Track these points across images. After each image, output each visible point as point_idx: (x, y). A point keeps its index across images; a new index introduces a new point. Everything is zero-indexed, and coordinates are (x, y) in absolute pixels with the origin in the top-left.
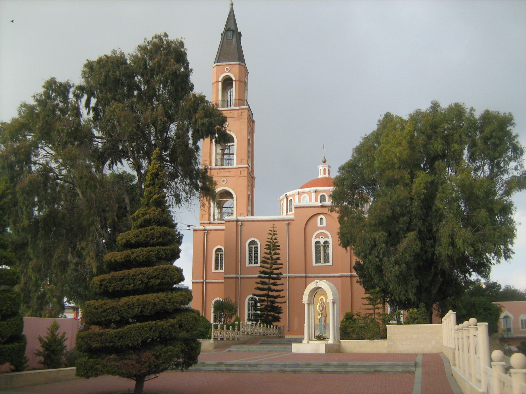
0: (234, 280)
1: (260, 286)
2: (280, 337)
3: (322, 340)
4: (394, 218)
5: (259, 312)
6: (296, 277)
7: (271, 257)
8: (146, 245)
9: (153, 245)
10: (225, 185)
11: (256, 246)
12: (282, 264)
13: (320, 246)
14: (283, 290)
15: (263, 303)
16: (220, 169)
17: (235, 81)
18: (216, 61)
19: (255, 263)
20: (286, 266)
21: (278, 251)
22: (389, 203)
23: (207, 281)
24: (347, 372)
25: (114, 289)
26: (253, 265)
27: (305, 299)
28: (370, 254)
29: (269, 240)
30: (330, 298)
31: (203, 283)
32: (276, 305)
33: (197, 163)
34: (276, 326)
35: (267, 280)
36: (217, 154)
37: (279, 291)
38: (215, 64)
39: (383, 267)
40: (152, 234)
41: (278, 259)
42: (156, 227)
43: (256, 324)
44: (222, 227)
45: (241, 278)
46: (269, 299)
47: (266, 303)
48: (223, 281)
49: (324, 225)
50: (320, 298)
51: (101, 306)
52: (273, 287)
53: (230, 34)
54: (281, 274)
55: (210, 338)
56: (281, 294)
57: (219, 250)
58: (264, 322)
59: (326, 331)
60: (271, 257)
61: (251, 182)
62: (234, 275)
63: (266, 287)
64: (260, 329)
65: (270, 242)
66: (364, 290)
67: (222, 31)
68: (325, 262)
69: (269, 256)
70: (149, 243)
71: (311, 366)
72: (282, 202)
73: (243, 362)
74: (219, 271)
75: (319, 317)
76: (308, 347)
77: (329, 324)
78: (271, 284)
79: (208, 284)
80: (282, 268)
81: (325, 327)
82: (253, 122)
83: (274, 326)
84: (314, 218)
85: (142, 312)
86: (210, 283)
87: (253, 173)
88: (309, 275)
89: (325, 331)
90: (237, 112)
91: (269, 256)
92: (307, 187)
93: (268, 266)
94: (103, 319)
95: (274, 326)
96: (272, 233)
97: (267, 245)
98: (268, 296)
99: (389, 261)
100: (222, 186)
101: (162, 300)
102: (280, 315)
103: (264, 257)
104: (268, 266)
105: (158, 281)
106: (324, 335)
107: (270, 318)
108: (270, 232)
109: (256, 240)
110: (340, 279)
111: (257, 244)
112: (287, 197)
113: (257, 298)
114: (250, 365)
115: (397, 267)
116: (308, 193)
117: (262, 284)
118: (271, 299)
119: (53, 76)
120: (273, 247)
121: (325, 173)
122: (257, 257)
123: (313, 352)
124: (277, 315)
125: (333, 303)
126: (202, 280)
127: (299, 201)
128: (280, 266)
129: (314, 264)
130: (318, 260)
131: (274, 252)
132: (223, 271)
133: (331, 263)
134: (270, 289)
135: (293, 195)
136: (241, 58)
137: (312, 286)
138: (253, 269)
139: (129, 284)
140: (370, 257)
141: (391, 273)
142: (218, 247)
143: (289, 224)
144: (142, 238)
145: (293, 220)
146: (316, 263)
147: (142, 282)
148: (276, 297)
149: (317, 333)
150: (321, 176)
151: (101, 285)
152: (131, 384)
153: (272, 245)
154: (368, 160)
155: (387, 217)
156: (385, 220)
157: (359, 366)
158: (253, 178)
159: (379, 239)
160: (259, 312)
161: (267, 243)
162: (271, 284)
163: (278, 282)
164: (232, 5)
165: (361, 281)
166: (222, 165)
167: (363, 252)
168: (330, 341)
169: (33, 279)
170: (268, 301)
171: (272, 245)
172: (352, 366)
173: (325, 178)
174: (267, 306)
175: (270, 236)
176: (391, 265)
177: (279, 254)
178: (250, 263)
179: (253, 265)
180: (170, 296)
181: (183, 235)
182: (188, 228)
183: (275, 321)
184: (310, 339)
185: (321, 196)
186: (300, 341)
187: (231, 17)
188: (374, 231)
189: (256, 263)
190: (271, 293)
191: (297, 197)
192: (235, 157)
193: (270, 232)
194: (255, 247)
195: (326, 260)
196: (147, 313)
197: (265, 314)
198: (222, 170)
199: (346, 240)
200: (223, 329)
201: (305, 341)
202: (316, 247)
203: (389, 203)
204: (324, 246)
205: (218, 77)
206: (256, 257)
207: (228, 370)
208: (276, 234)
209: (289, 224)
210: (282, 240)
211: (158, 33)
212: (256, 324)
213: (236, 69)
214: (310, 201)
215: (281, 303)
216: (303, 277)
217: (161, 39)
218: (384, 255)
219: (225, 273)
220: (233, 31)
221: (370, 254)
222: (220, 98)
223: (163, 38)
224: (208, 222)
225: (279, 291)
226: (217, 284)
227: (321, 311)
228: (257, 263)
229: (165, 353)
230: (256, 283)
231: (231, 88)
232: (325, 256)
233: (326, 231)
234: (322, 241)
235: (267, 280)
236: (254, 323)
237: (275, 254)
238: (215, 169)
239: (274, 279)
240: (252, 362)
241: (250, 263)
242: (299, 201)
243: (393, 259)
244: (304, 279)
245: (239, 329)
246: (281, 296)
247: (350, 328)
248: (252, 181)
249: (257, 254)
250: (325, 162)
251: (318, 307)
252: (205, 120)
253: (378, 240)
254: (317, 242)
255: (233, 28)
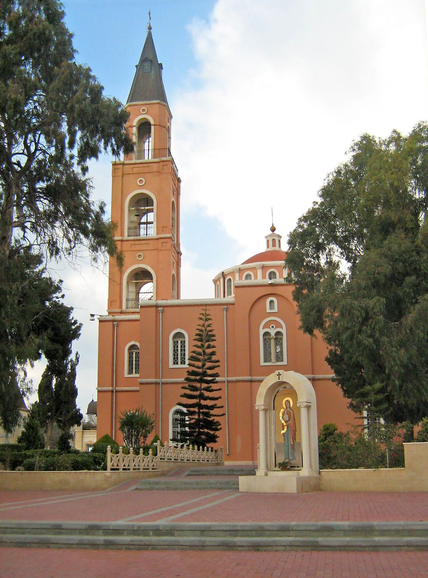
0: (154, 385)
1: (188, 392)
2: (218, 464)
3: (289, 470)
4: (396, 279)
5: (187, 429)
6: (238, 381)
7: (204, 351)
11: (182, 340)
12: (218, 361)
13: (270, 339)
14: (220, 398)
15: (193, 417)
16: (134, 240)
17: (154, 125)
18: (129, 100)
19: (181, 364)
20: (224, 364)
21: (212, 343)
23: (118, 388)
24: (375, 548)
26: (179, 366)
27: (260, 402)
28: (360, 331)
29: (200, 328)
34: (212, 448)
35: (198, 385)
37: (217, 399)
38: (128, 104)
39: (381, 352)
41: (213, 353)
43: (182, 447)
44: (137, 317)
45: (162, 384)
46: (201, 411)
47: (196, 417)
49: (276, 310)
52: (206, 394)
53: (147, 65)
54: (217, 375)
55: (105, 468)
56: (218, 403)
58: (193, 443)
60: (204, 351)
61: (176, 258)
62: (154, 380)
63: (197, 393)
64: (190, 453)
65: (201, 331)
66: (343, 393)
68: (277, 361)
69: (200, 350)
71: (291, 533)
72: (218, 283)
75: (283, 432)
76: (267, 480)
77: (300, 444)
78: (204, 389)
80: (219, 366)
81: (293, 447)
82: (179, 180)
83: (208, 448)
84: (262, 300)
86: (122, 391)
89: (293, 456)
90: (156, 165)
91: (200, 350)
93: (200, 364)
95: (208, 448)
97: (197, 335)
98: (200, 406)
99: (390, 343)
100: (137, 263)
102: (217, 433)
103: (194, 352)
104: (200, 364)
106: (293, 462)
107: (203, 437)
108: (201, 316)
111: (184, 337)
113: (185, 410)
114: (157, 531)
115: (403, 351)
116: (254, 269)
117: (191, 390)
118: (205, 410)
121: (274, 245)
124: (212, 432)
128: (216, 364)
131: (207, 344)
134: (202, 397)
137: (271, 380)
138: (179, 370)
141: (394, 360)
145: (233, 304)
146: (265, 361)
148: (212, 407)
149: (281, 459)
153: (204, 335)
156: (383, 280)
157: (398, 532)
160: (187, 429)
161: (198, 332)
162: (204, 389)
163: (214, 386)
164: (150, 28)
165: (338, 379)
168: (305, 472)
170: (199, 413)
172: (383, 532)
174: (198, 420)
176: (394, 349)
177: (214, 347)
178: (174, 364)
179: (179, 366)
181: (81, 324)
182: (92, 318)
183: (209, 442)
185: (271, 273)
186: (251, 472)
187: (149, 43)
189: (183, 362)
190: (203, 402)
193: (201, 316)
194: (181, 342)
197: (195, 432)
198: (138, 242)
200: (117, 452)
201: (261, 471)
202: (265, 340)
204: (276, 339)
207: (108, 544)
208: (210, 319)
210: (219, 328)
212: (182, 447)
215: (218, 416)
218: (382, 334)
224: (120, 310)
225: (217, 399)
227: (286, 422)
230: (183, 388)
231: (150, 137)
234: (273, 332)
235: (198, 385)
236: (180, 444)
237: (209, 347)
238: (128, 240)
239: (207, 382)
240: (162, 522)
241: (175, 363)
243: (396, 338)
244: (249, 384)
245: (155, 454)
246: (218, 405)
247: (333, 451)
248: (178, 257)
249: (184, 350)
251: (281, 415)
253: (373, 308)
254: (266, 334)
255: (151, 57)
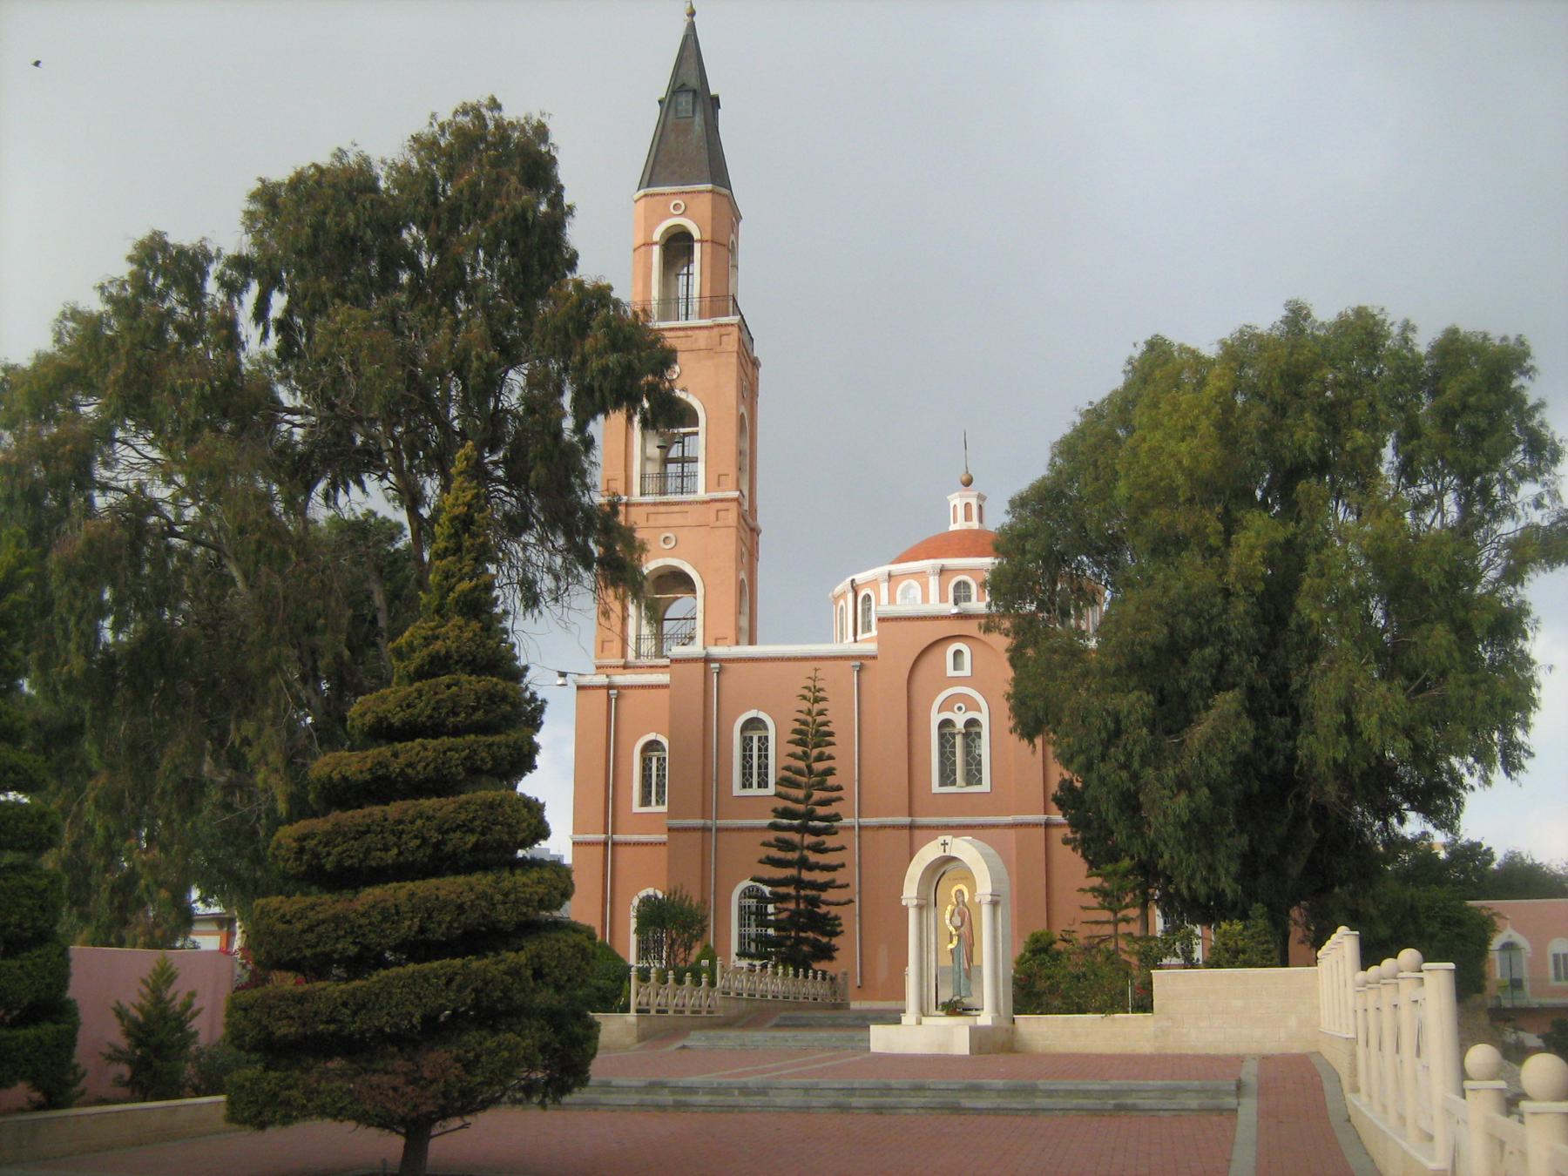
0: (699, 834)
1: (775, 853)
2: (836, 1007)
3: (960, 1014)
4: (1175, 650)
5: (771, 931)
6: (882, 827)
7: (809, 767)
8: (435, 730)
9: (456, 732)
10: (671, 552)
11: (762, 733)
12: (839, 788)
13: (953, 736)
14: (843, 866)
15: (785, 906)
16: (655, 504)
17: (701, 241)
18: (645, 182)
19: (759, 786)
20: (852, 793)
21: (827, 750)
22: (1159, 607)
23: (617, 837)
24: (1035, 1111)
25: (339, 864)
26: (755, 791)
27: (910, 893)
28: (1103, 757)
29: (802, 716)
30: (984, 888)
31: (606, 844)
32: (823, 909)
33: (586, 488)
34: (824, 973)
35: (795, 837)
36: (645, 459)
37: (833, 868)
38: (642, 192)
39: (1141, 798)
40: (453, 698)
41: (830, 772)
42: (464, 678)
43: (764, 967)
44: (663, 678)
45: (718, 830)
46: (802, 893)
47: (792, 906)
48: (664, 837)
49: (966, 671)
50: (952, 889)
51: (302, 914)
52: (813, 857)
53: (685, 100)
54: (837, 817)
55: (626, 1009)
56: (839, 877)
57: (652, 746)
58: (786, 960)
59: (973, 987)
60: (809, 767)
61: (748, 542)
62: (699, 822)
63: (793, 856)
64: (776, 982)
65: (804, 723)
66: (1086, 866)
67: (662, 92)
68: (969, 783)
69: (801, 764)
70: (443, 724)
71: (928, 1093)
72: (842, 602)
73: (725, 1081)
74: (654, 808)
75: (951, 946)
76: (918, 1034)
77: (980, 968)
78: (808, 848)
79: (620, 849)
80: (840, 799)
81: (968, 976)
82: (755, 364)
83: (815, 973)
84: (937, 651)
85: (422, 930)
86: (627, 844)
87: (754, 517)
88: (921, 820)
89: (968, 989)
90: (705, 333)
91: (801, 764)
92: (916, 559)
93: (800, 794)
94: (308, 952)
95: (815, 973)
96: (810, 695)
97: (795, 731)
98: (799, 883)
99: (1159, 779)
100: (663, 556)
101: (483, 896)
102: (835, 941)
103: (788, 768)
104: (800, 794)
105: (472, 839)
106: (966, 1001)
107: (805, 948)
108: (805, 692)
109: (763, 716)
110: (1012, 832)
111: (766, 728)
112: (855, 588)
113: (767, 890)
114: (745, 1090)
115: (1183, 798)
116: (919, 575)
117: (780, 849)
118: (809, 892)
119: (159, 228)
120: (812, 736)
121: (968, 517)
122: (766, 767)
123: (934, 1051)
124: (825, 940)
125: (994, 904)
126: (602, 837)
127: (892, 600)
128: (835, 794)
129: (936, 788)
130: (947, 777)
131: (815, 752)
132: (664, 809)
133: (985, 786)
134: (803, 864)
135: (874, 583)
136: (717, 173)
137: (929, 852)
138: (754, 802)
139: (386, 849)
140: (1103, 768)
141: (1165, 815)
142: (651, 736)
143: (861, 669)
144: (423, 711)
145: (874, 657)
146: (942, 784)
147: (424, 841)
148: (824, 887)
149: (946, 995)
150: (958, 525)
151: (302, 850)
152: (392, 1145)
153: (811, 730)
154: (1097, 479)
155: (1154, 647)
156: (1148, 655)
157: (1069, 1093)
158: (755, 531)
159: (1129, 713)
160: (771, 931)
161: (797, 725)
162: (808, 848)
163: (830, 841)
164: (692, 14)
165: (1075, 839)
166: (663, 492)
167: (1081, 751)
168: (985, 1019)
169: (100, 832)
170: (797, 899)
171: (811, 730)
172: (1050, 1093)
173: (970, 532)
174: (796, 914)
175: (805, 705)
176: (1167, 792)
177: (830, 758)
178: (744, 786)
179: (755, 791)
180: (506, 885)
181: (544, 701)
182: (560, 681)
183: (819, 958)
184: (923, 1012)
185: (958, 585)
186: (894, 1018)
187: (690, 50)
188: (1115, 689)
189: (763, 784)
190: (806, 876)
191: (884, 587)
192: (701, 467)
193: (805, 692)
194: (760, 739)
195: (973, 777)
196: (438, 933)
197: (789, 937)
198: (662, 509)
199: (1031, 716)
200: (666, 982)
201: (909, 1018)
202: (942, 736)
203: (1159, 607)
204: (966, 735)
205: (650, 230)
206: (763, 768)
207: (678, 1106)
208: (824, 699)
209: (861, 669)
210: (841, 717)
211: (472, 100)
212: (764, 967)
213: (704, 205)
214: (925, 599)
215: (838, 904)
216: (902, 827)
217: (479, 117)
218: (1144, 762)
219: (671, 814)
220: (695, 92)
221: (1103, 757)
222: (655, 293)
223: (487, 114)
224: (621, 662)
225: (833, 868)
226: (646, 849)
227: (957, 928)
228: (766, 786)
229: (491, 1053)
230: (764, 844)
231: (690, 261)
232: (968, 764)
233: (972, 688)
234: (960, 720)
235: (795, 837)
236: (757, 963)
237: (820, 758)
238: (640, 504)
239: (817, 832)
240: (752, 1080)
241: (746, 784)
242: (892, 600)
243: (1170, 773)
244: (906, 832)
245: (712, 983)
246: (839, 882)
247: (1042, 980)
248: (752, 539)
249: (766, 757)
250: (968, 483)
251: (947, 916)
252: (612, 359)
253: (1127, 717)
254: (946, 723)
255: (693, 82)
